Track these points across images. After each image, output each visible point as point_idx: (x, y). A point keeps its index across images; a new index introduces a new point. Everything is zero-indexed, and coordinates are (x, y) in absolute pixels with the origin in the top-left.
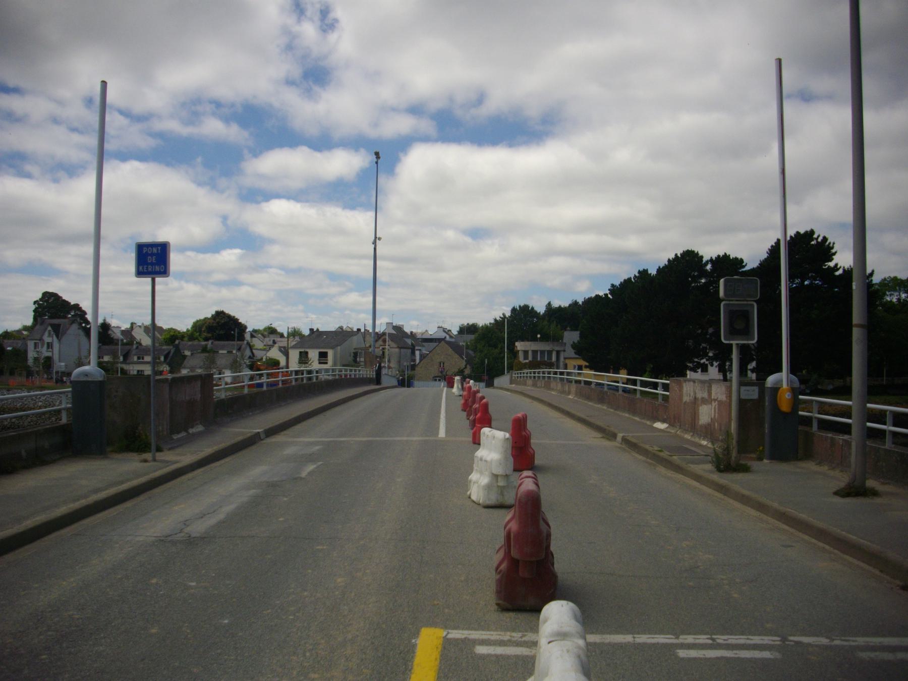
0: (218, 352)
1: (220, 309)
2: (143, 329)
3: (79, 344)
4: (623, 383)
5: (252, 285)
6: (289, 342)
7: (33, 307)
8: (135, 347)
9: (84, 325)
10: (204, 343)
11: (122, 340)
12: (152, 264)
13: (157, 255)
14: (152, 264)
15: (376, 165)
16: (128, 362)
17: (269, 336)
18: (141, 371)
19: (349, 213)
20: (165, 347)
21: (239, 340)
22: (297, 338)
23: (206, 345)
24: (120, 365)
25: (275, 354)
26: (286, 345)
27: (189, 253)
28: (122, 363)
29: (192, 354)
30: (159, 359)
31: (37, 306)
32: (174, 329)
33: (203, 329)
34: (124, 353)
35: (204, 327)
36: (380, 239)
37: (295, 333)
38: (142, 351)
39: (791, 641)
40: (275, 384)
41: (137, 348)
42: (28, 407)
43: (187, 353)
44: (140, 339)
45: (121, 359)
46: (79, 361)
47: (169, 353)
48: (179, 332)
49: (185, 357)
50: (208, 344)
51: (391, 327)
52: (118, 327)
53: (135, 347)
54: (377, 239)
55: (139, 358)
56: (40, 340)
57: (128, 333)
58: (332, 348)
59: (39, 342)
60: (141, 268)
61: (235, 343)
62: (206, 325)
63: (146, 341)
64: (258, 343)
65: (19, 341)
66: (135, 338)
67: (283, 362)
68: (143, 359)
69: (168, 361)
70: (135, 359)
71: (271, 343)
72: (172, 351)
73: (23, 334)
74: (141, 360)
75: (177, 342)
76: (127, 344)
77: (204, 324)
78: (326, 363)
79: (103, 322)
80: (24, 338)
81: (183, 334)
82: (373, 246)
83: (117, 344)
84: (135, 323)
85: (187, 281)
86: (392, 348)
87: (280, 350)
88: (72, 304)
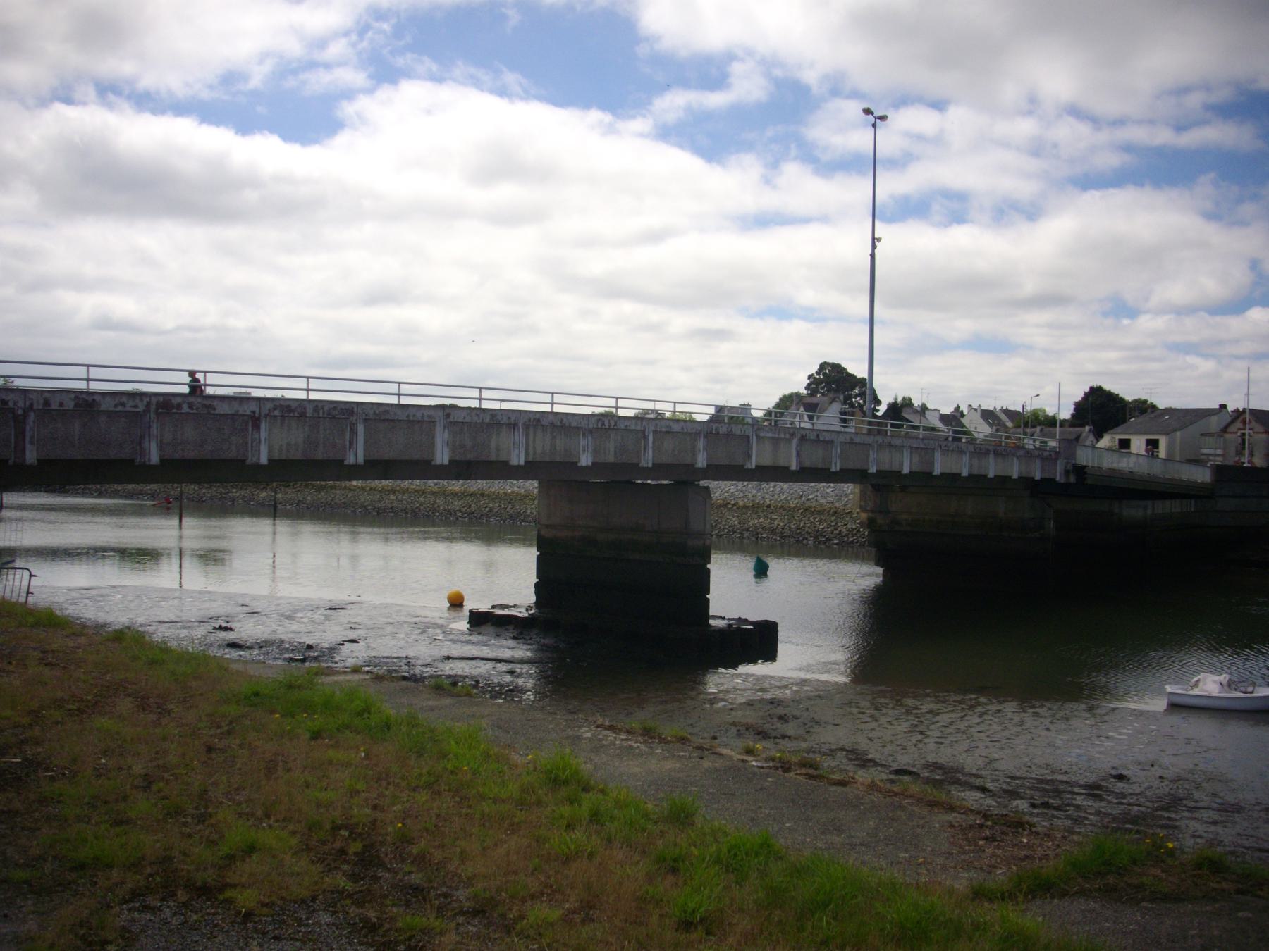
1: (1095, 384)
2: (979, 412)
4: (1249, 440)
36: (879, 240)
42: (362, 715)
58: (1167, 434)
86: (1257, 433)
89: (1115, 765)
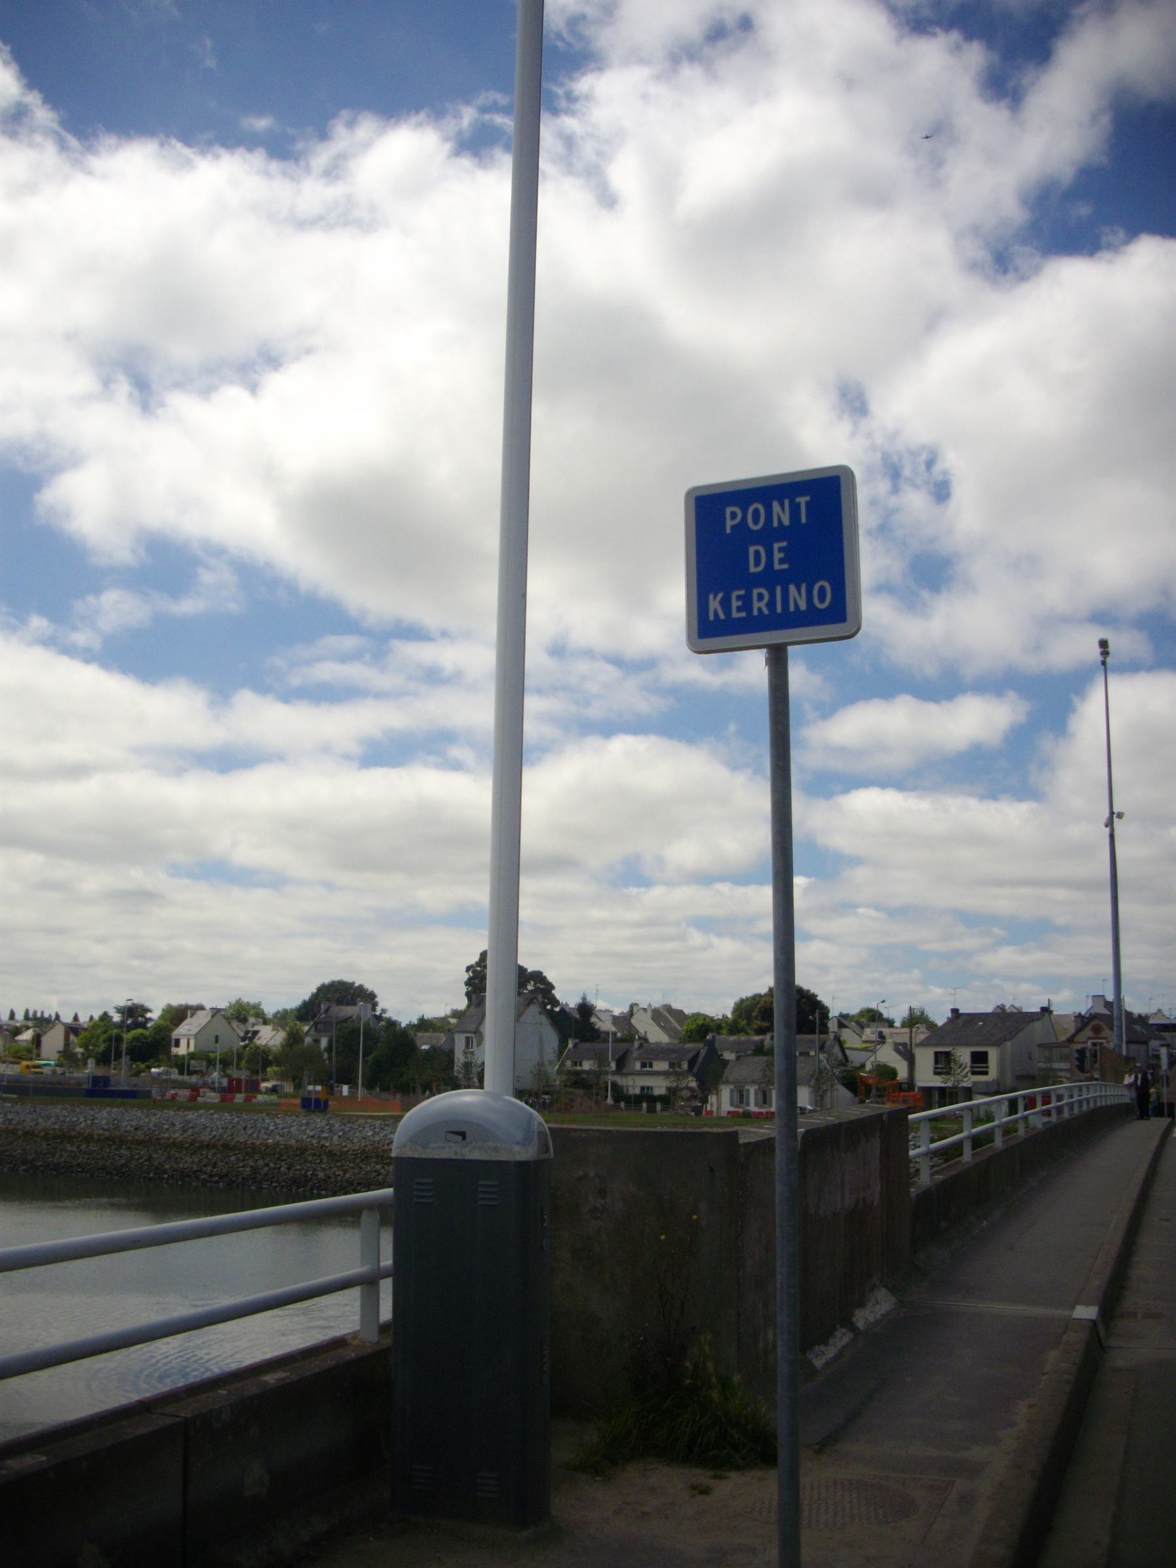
0: (809, 1053)
2: (649, 1013)
3: (541, 1041)
5: (827, 939)
6: (913, 1034)
7: (466, 976)
8: (636, 1044)
9: (549, 1007)
10: (757, 1038)
11: (614, 1034)
12: (769, 579)
13: (791, 533)
14: (769, 579)
15: (1103, 667)
16: (624, 1071)
17: (868, 1026)
18: (648, 1088)
19: (991, 806)
20: (689, 1046)
21: (821, 1032)
22: (922, 1028)
23: (762, 1042)
24: (610, 1078)
25: (888, 1056)
26: (907, 1040)
27: (720, 886)
28: (614, 1073)
29: (738, 1058)
30: (679, 1066)
31: (471, 975)
32: (703, 1015)
33: (754, 1014)
34: (617, 1056)
35: (756, 1010)
36: (1120, 815)
37: (915, 1020)
38: (651, 1052)
39: (767, 1129)
40: (987, 1137)
41: (641, 1046)
43: (729, 1056)
44: (646, 1032)
45: (613, 1065)
46: (540, 1070)
47: (697, 1055)
48: (712, 1019)
49: (725, 1063)
50: (766, 1038)
51: (1102, 1004)
52: (607, 1011)
53: (636, 1044)
54: (1115, 816)
55: (644, 1065)
56: (475, 1033)
57: (624, 1021)
58: (996, 1044)
59: (473, 1035)
60: (714, 604)
61: (815, 1037)
62: (759, 1006)
63: (657, 1035)
64: (850, 1038)
65: (442, 1035)
66: (637, 1032)
67: (902, 1074)
68: (651, 1066)
69: (695, 1070)
70: (638, 1066)
71: (874, 1037)
72: (703, 1053)
73: (450, 1023)
74: (648, 1069)
75: (709, 1037)
76: (622, 1040)
77: (756, 1005)
78: (986, 1073)
79: (581, 1001)
80: (449, 1030)
81: (719, 1022)
82: (1107, 830)
83: (606, 1041)
84: (636, 1004)
85: (719, 935)
87: (897, 1050)
88: (529, 971)
89: (700, 1497)
